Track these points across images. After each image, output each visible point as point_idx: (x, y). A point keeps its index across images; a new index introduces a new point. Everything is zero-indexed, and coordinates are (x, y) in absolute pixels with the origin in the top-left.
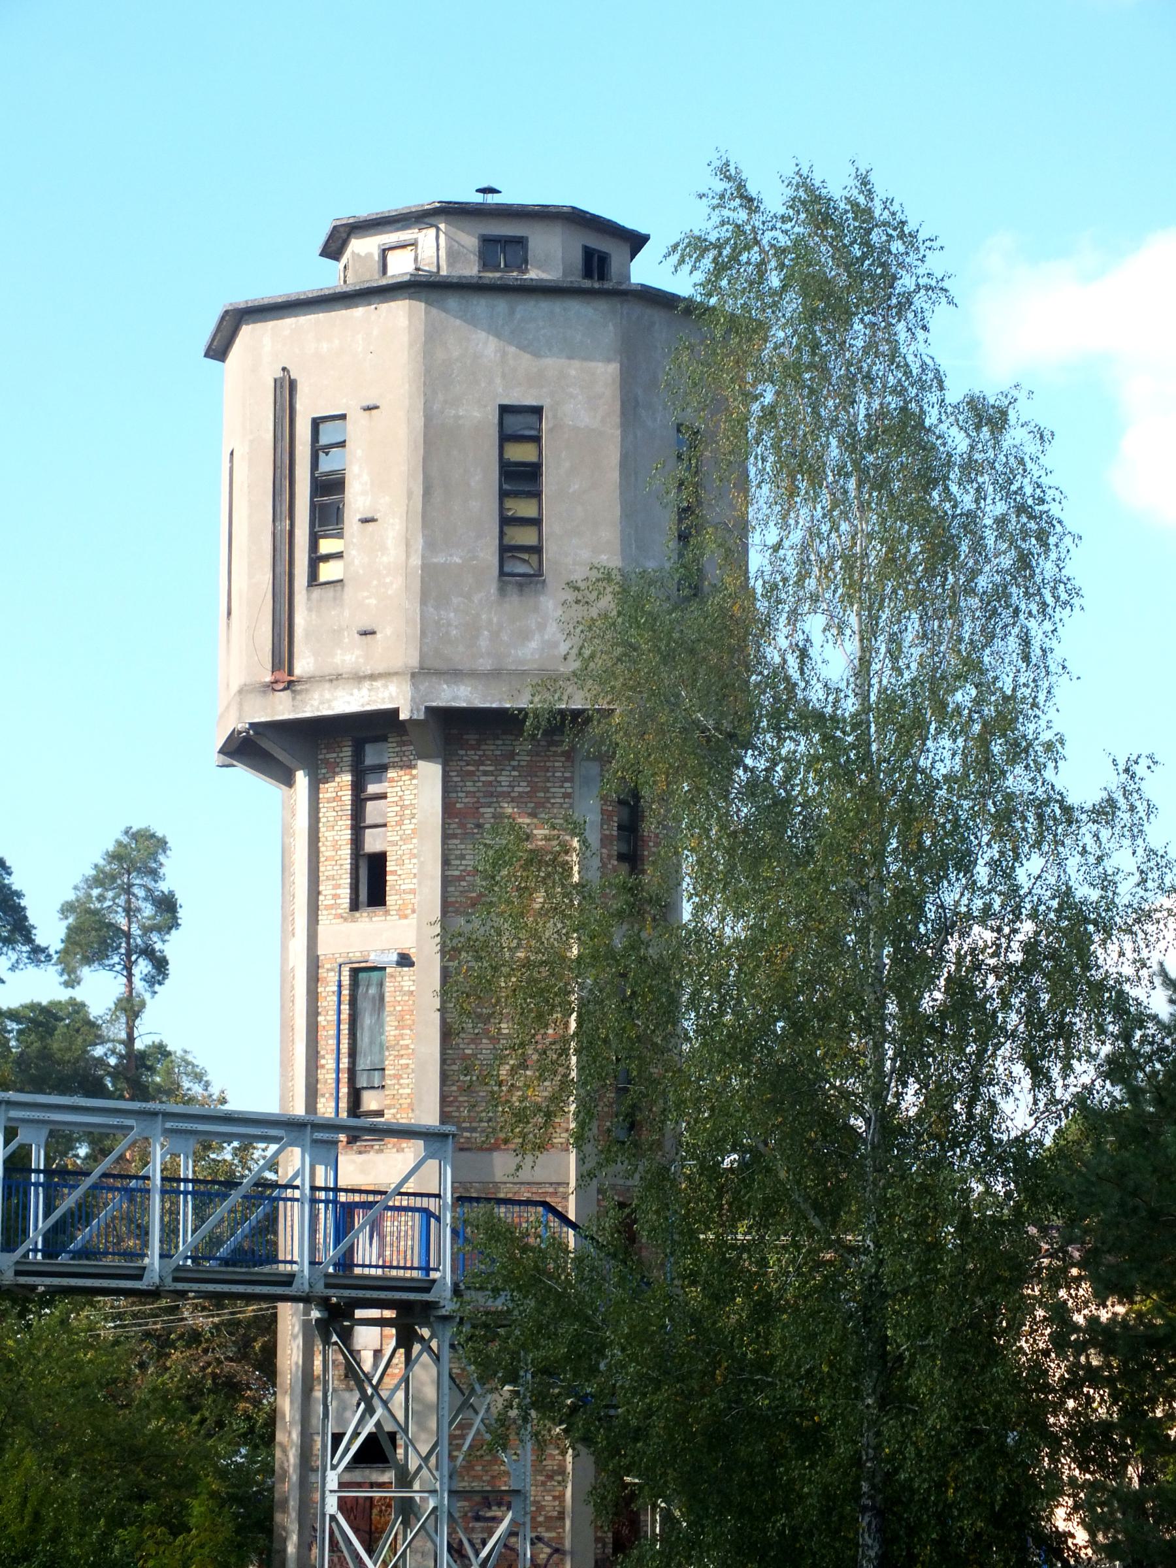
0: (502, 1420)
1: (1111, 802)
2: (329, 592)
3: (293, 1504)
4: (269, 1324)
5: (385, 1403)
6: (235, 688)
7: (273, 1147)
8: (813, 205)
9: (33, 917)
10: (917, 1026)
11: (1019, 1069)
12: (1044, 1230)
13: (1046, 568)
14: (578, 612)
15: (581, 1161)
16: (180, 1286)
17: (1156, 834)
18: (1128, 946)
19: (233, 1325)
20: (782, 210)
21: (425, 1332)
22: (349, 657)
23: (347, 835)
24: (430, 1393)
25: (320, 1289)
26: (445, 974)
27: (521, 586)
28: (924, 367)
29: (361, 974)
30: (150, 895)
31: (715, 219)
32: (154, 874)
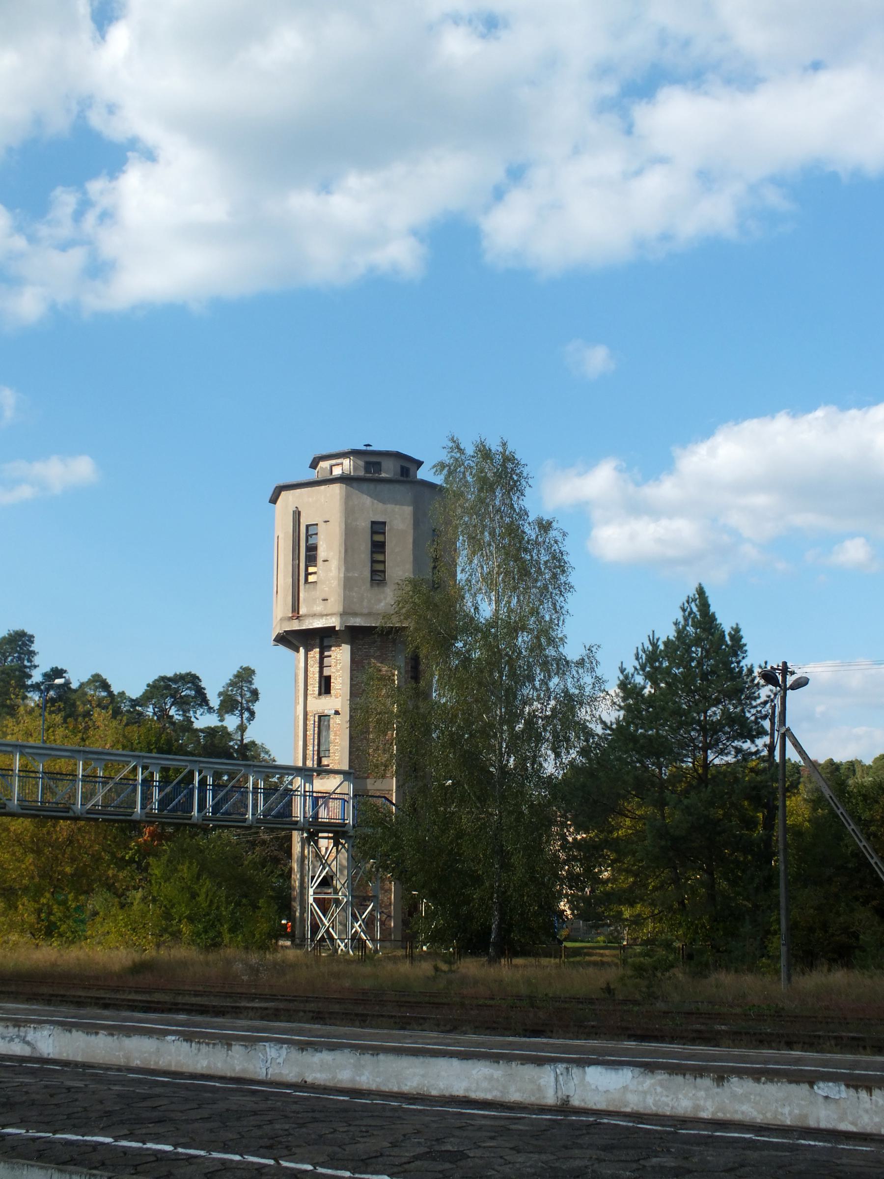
0: (370, 871)
1: (583, 659)
2: (312, 586)
3: (298, 899)
4: (289, 838)
5: (329, 866)
6: (279, 618)
7: (291, 778)
8: (485, 454)
9: (209, 697)
10: (515, 737)
11: (549, 752)
12: (558, 808)
13: (563, 579)
14: (400, 592)
15: (397, 782)
16: (259, 825)
17: (599, 672)
18: (588, 710)
19: (277, 838)
20: (472, 454)
21: (343, 841)
22: (318, 608)
23: (317, 669)
24: (345, 863)
25: (307, 826)
26: (351, 717)
27: (378, 584)
28: (521, 509)
29: (322, 718)
30: (249, 690)
31: (449, 456)
32: (251, 683)
